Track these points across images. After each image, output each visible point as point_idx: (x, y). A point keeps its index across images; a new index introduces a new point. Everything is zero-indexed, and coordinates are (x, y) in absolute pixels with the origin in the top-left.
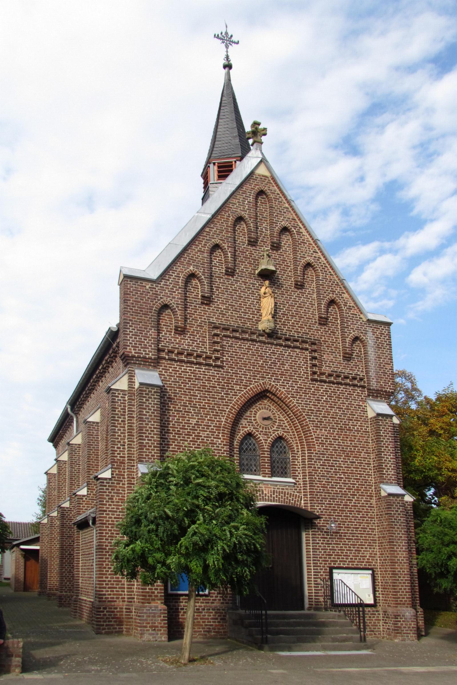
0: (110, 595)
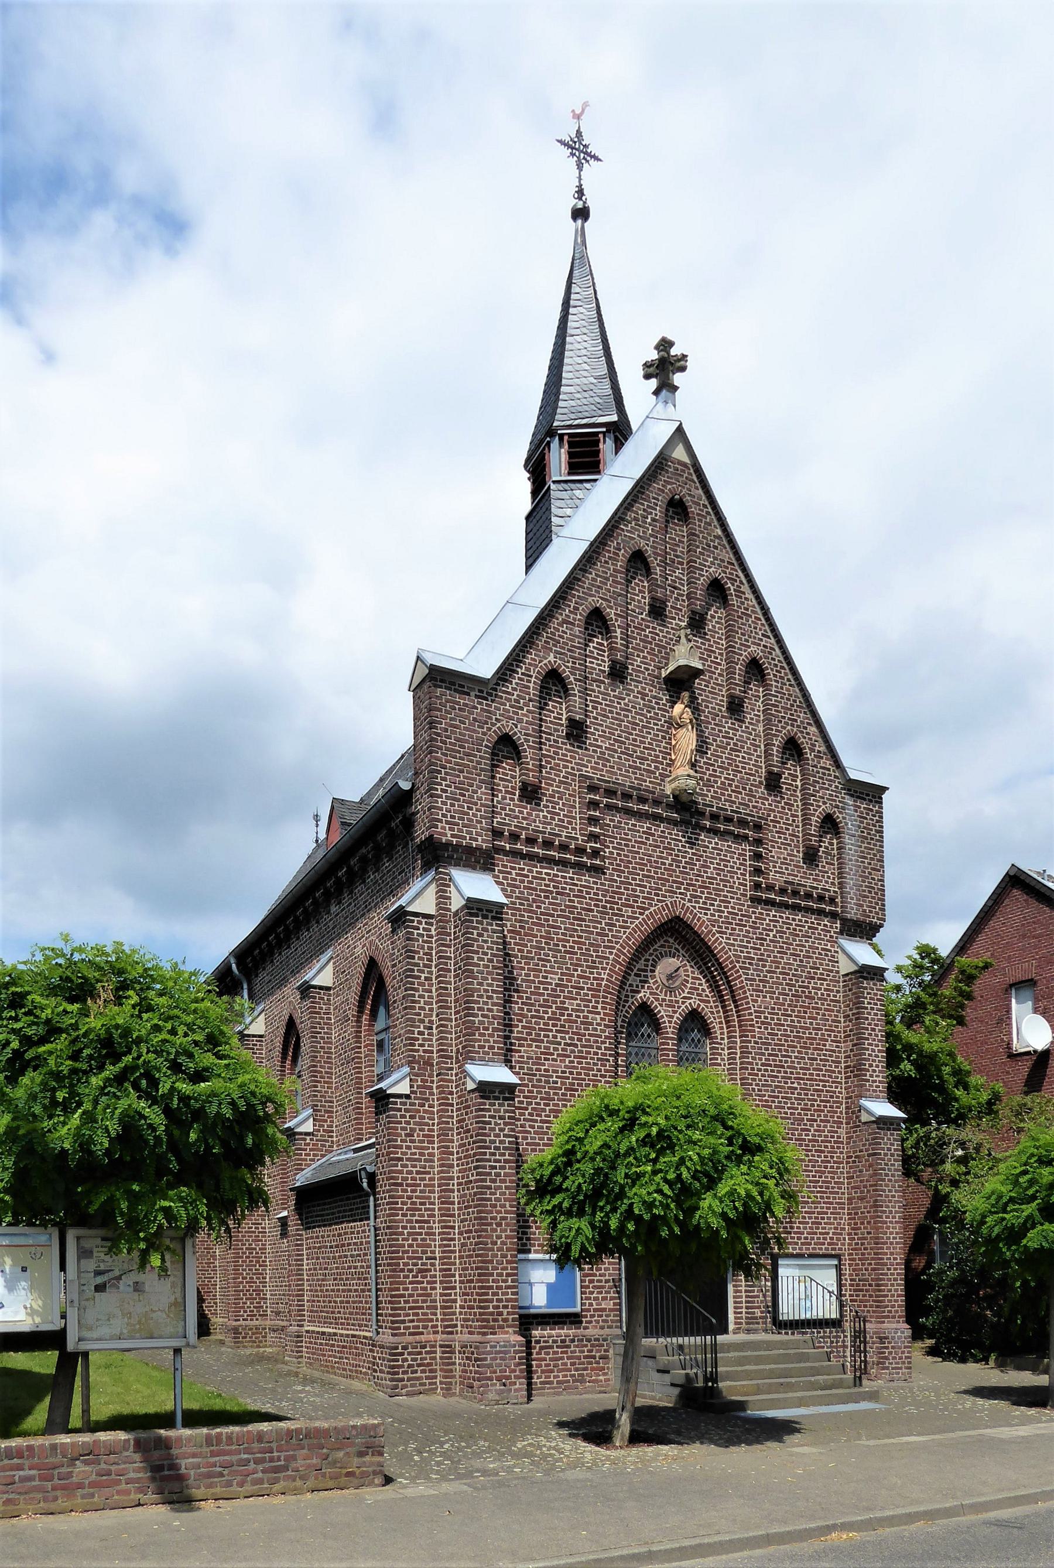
0: (412, 1321)
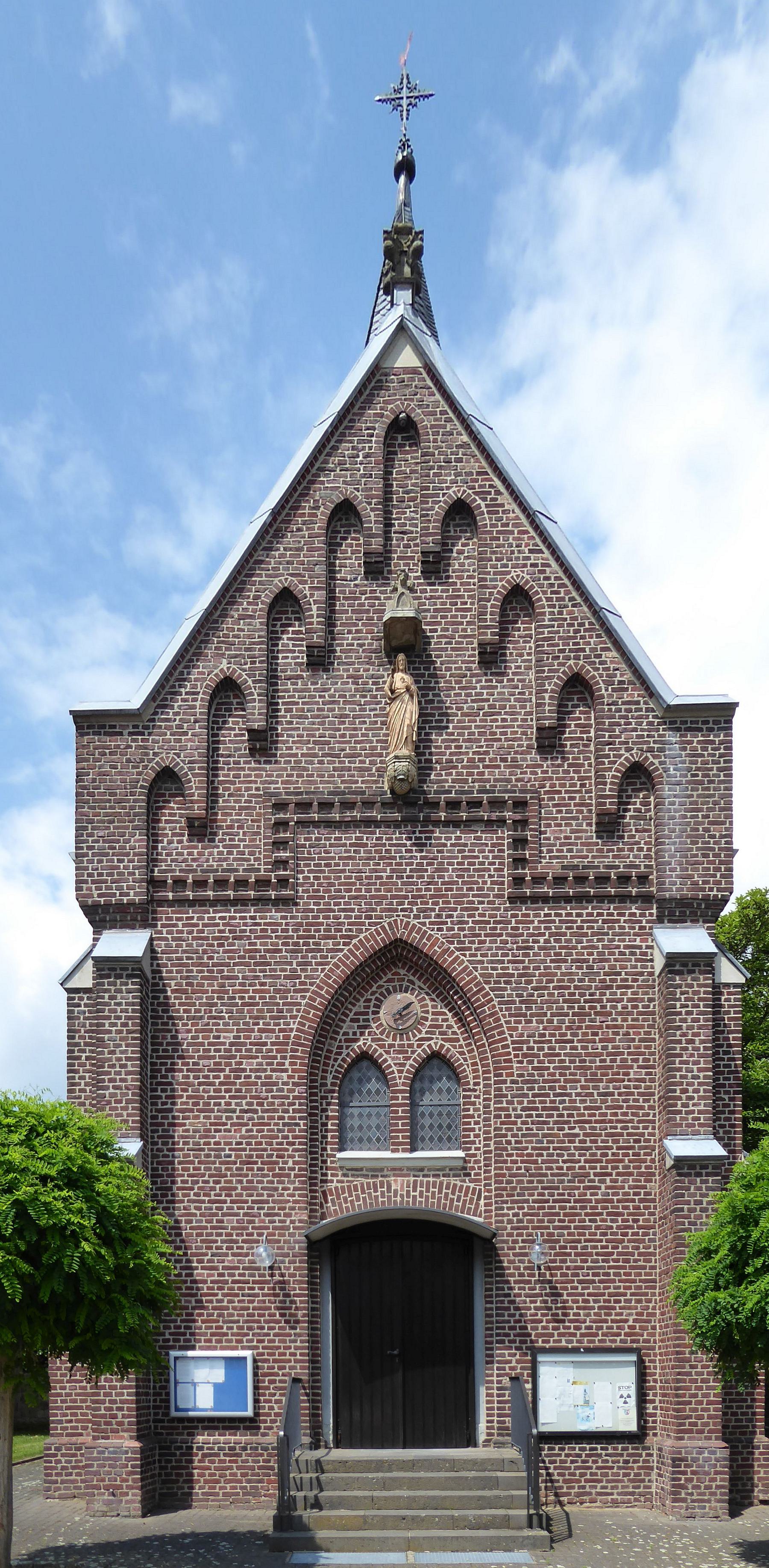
0: (71, 1421)
